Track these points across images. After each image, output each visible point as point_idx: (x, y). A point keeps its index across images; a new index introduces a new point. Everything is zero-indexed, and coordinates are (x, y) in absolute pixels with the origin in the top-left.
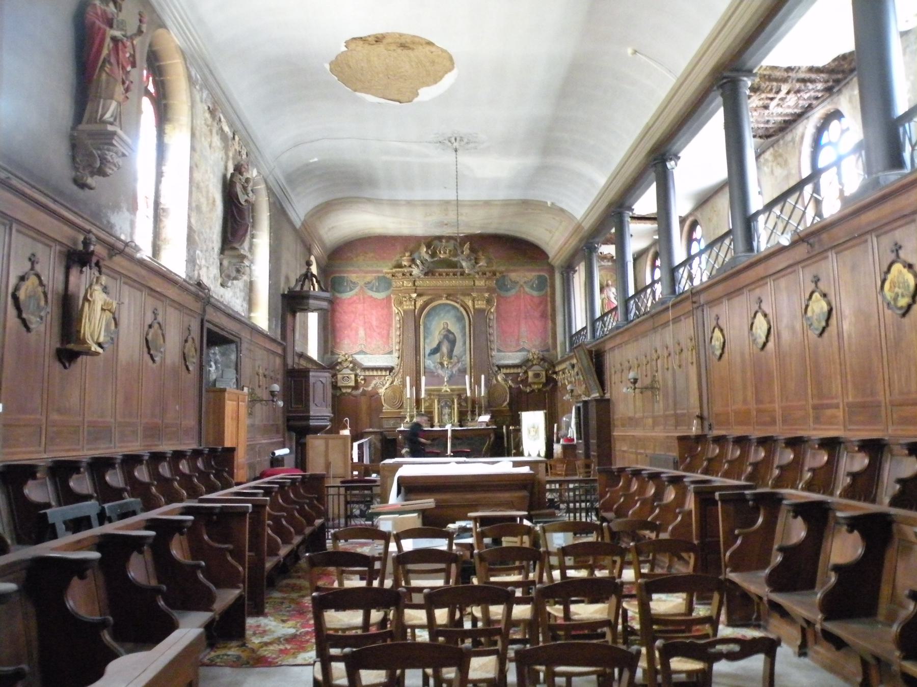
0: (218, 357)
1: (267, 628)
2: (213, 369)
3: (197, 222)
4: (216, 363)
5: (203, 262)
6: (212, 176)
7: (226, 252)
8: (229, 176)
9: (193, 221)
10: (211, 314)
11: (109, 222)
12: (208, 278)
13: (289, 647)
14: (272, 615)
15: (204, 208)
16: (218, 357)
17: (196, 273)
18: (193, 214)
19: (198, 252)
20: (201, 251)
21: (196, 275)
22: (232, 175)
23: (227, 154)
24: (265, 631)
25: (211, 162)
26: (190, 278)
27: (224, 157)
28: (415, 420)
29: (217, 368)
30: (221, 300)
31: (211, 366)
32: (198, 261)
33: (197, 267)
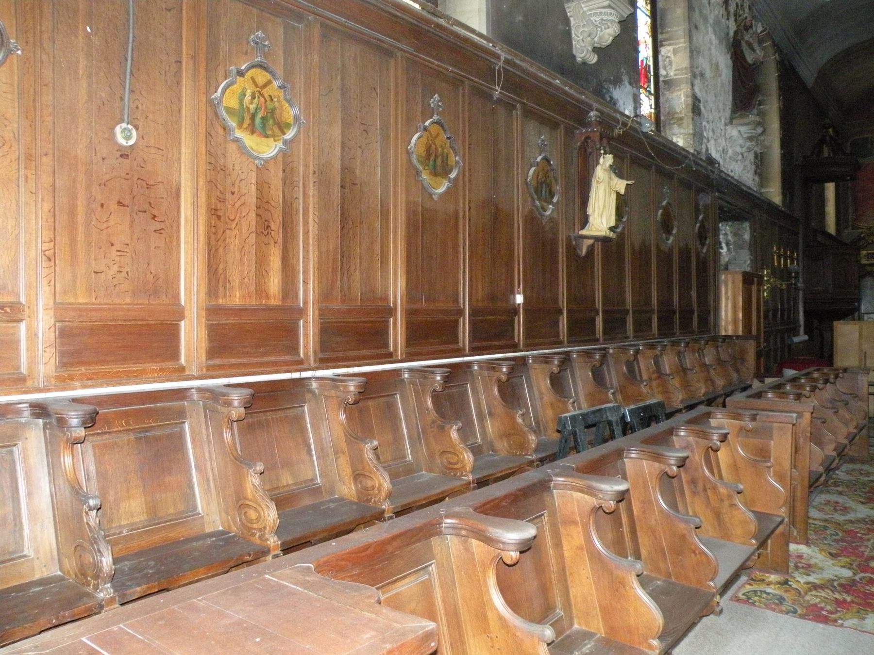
0: (730, 238)
1: (812, 562)
2: (724, 251)
3: (700, 91)
4: (727, 244)
5: (711, 134)
6: (713, 37)
7: (734, 121)
8: (732, 34)
9: (697, 90)
10: (722, 174)
11: (611, 98)
12: (717, 151)
13: (849, 599)
14: (816, 545)
15: (708, 74)
16: (730, 238)
17: (704, 146)
18: (697, 82)
19: (704, 123)
20: (708, 122)
21: (704, 150)
22: (736, 32)
23: (727, 9)
24: (809, 566)
25: (711, 21)
26: (699, 153)
27: (725, 13)
28: (82, 432)
29: (729, 250)
30: (732, 174)
31: (722, 248)
32: (705, 134)
33: (705, 141)
